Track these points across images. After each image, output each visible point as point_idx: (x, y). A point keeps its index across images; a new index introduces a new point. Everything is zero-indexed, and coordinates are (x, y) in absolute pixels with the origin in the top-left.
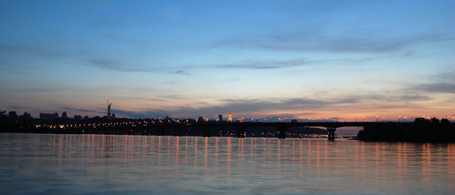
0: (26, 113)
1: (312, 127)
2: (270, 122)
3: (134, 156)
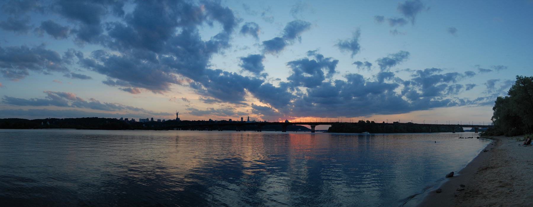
0: (210, 119)
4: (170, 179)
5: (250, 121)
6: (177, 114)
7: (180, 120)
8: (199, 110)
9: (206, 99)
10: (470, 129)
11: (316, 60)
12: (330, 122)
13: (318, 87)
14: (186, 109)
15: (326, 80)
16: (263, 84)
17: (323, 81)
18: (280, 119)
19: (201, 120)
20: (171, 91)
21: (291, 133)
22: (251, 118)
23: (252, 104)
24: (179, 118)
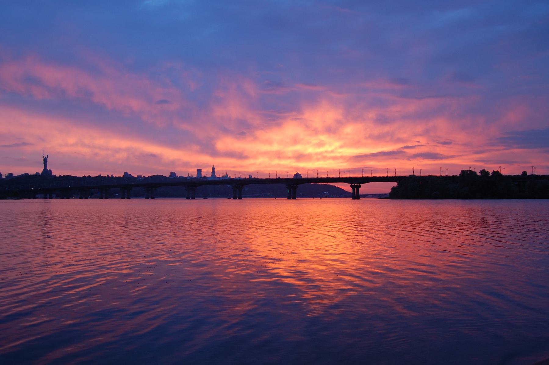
0: (126, 173)
1: (320, 184)
2: (387, 176)
4: (108, 266)
5: (217, 175)
6: (45, 161)
7: (53, 174)
10: (387, 188)
24: (50, 170)
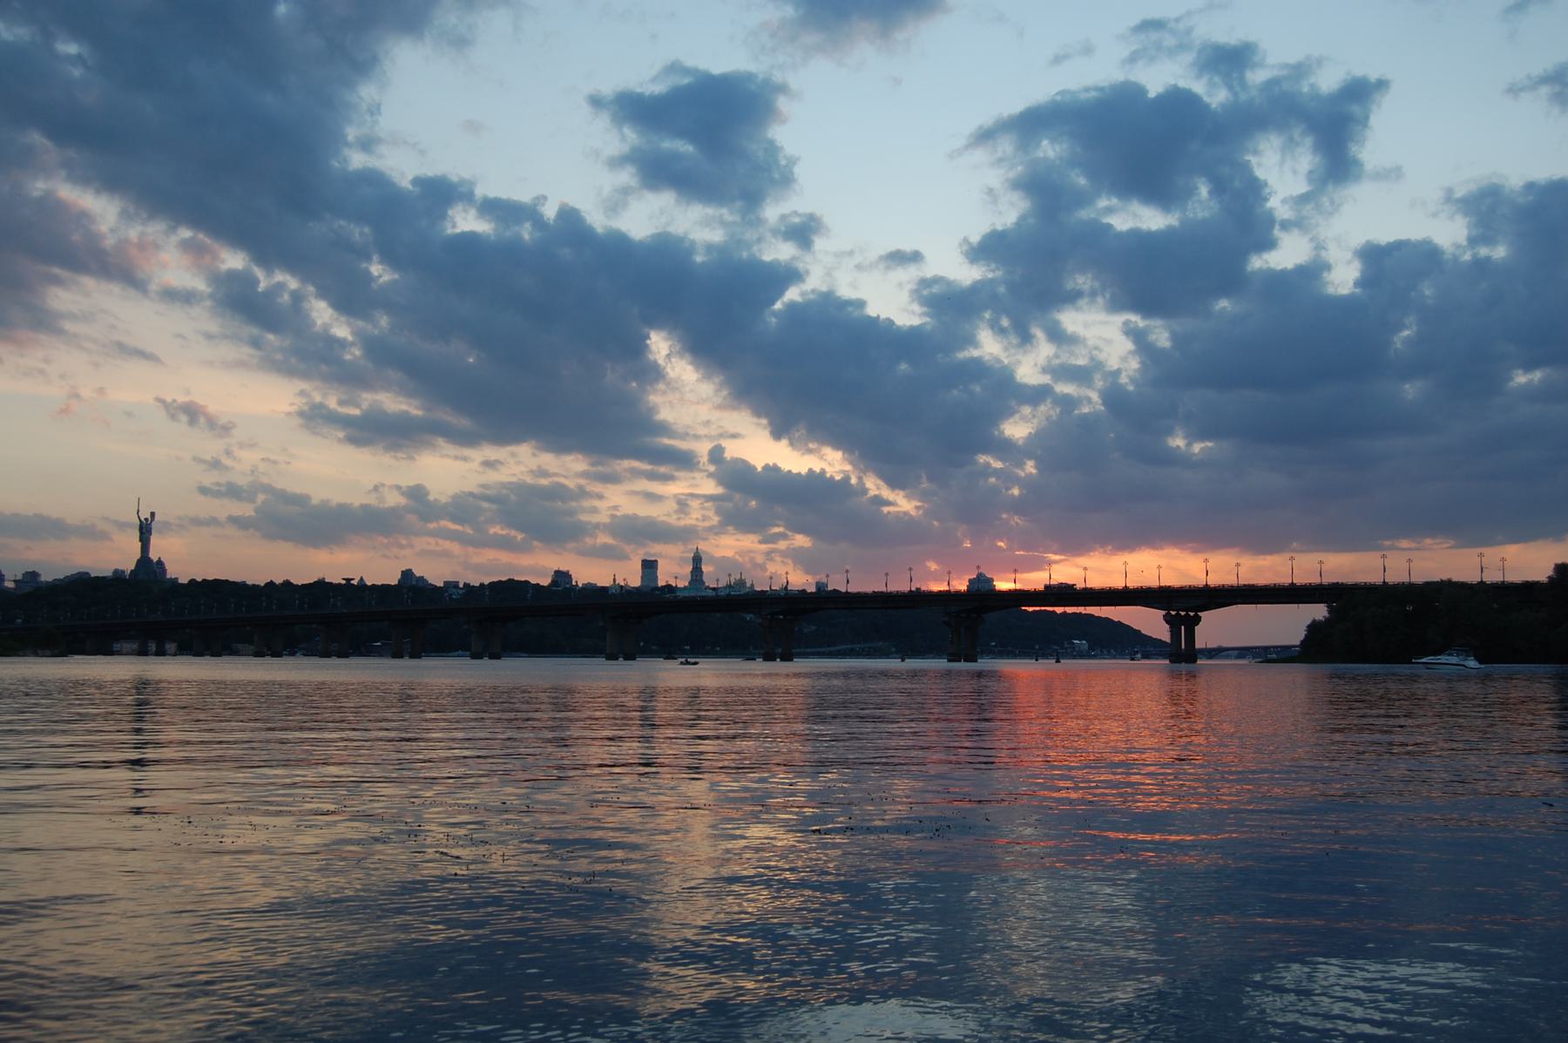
0: (407, 574)
1: (1059, 610)
3: (878, 725)
5: (710, 582)
6: (145, 530)
8: (315, 501)
9: (357, 412)
11: (1199, 87)
12: (1315, 580)
13: (1223, 304)
14: (203, 490)
15: (1287, 254)
16: (792, 294)
17: (1258, 263)
18: (933, 566)
19: (336, 578)
20: (58, 332)
21: (1022, 671)
22: (712, 560)
23: (716, 455)
24: (160, 562)
